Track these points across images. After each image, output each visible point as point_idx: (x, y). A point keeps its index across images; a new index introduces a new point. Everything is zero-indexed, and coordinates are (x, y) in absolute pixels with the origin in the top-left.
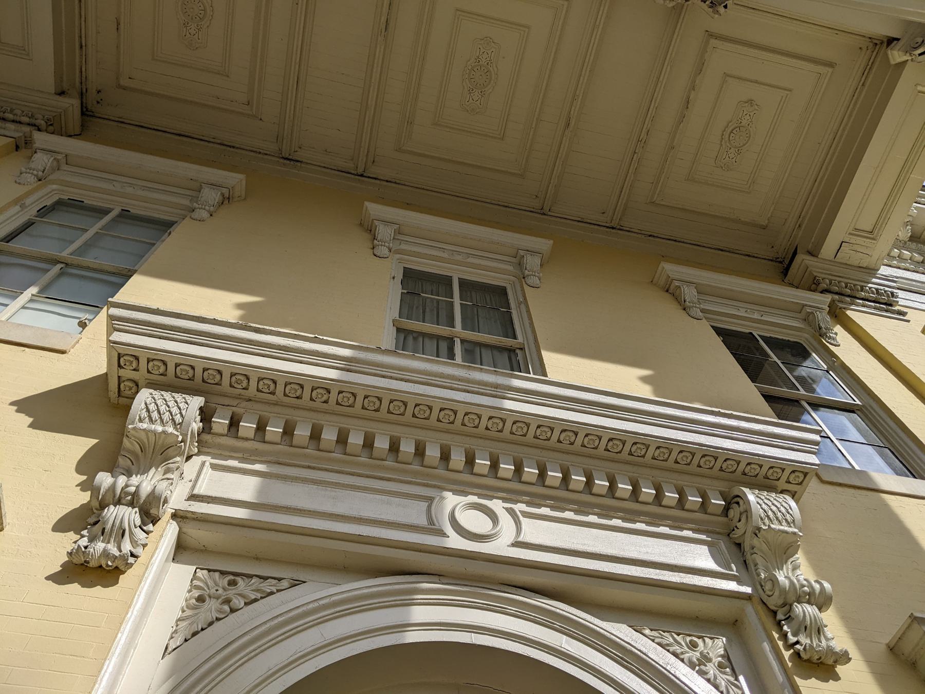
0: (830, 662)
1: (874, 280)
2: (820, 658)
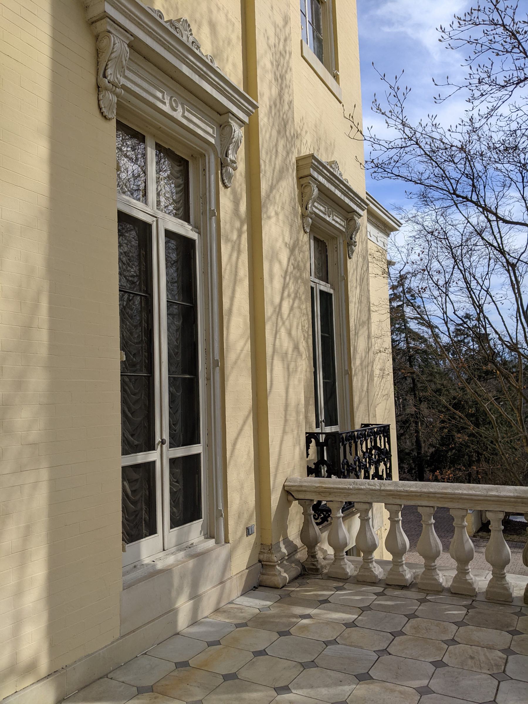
1: (383, 447)
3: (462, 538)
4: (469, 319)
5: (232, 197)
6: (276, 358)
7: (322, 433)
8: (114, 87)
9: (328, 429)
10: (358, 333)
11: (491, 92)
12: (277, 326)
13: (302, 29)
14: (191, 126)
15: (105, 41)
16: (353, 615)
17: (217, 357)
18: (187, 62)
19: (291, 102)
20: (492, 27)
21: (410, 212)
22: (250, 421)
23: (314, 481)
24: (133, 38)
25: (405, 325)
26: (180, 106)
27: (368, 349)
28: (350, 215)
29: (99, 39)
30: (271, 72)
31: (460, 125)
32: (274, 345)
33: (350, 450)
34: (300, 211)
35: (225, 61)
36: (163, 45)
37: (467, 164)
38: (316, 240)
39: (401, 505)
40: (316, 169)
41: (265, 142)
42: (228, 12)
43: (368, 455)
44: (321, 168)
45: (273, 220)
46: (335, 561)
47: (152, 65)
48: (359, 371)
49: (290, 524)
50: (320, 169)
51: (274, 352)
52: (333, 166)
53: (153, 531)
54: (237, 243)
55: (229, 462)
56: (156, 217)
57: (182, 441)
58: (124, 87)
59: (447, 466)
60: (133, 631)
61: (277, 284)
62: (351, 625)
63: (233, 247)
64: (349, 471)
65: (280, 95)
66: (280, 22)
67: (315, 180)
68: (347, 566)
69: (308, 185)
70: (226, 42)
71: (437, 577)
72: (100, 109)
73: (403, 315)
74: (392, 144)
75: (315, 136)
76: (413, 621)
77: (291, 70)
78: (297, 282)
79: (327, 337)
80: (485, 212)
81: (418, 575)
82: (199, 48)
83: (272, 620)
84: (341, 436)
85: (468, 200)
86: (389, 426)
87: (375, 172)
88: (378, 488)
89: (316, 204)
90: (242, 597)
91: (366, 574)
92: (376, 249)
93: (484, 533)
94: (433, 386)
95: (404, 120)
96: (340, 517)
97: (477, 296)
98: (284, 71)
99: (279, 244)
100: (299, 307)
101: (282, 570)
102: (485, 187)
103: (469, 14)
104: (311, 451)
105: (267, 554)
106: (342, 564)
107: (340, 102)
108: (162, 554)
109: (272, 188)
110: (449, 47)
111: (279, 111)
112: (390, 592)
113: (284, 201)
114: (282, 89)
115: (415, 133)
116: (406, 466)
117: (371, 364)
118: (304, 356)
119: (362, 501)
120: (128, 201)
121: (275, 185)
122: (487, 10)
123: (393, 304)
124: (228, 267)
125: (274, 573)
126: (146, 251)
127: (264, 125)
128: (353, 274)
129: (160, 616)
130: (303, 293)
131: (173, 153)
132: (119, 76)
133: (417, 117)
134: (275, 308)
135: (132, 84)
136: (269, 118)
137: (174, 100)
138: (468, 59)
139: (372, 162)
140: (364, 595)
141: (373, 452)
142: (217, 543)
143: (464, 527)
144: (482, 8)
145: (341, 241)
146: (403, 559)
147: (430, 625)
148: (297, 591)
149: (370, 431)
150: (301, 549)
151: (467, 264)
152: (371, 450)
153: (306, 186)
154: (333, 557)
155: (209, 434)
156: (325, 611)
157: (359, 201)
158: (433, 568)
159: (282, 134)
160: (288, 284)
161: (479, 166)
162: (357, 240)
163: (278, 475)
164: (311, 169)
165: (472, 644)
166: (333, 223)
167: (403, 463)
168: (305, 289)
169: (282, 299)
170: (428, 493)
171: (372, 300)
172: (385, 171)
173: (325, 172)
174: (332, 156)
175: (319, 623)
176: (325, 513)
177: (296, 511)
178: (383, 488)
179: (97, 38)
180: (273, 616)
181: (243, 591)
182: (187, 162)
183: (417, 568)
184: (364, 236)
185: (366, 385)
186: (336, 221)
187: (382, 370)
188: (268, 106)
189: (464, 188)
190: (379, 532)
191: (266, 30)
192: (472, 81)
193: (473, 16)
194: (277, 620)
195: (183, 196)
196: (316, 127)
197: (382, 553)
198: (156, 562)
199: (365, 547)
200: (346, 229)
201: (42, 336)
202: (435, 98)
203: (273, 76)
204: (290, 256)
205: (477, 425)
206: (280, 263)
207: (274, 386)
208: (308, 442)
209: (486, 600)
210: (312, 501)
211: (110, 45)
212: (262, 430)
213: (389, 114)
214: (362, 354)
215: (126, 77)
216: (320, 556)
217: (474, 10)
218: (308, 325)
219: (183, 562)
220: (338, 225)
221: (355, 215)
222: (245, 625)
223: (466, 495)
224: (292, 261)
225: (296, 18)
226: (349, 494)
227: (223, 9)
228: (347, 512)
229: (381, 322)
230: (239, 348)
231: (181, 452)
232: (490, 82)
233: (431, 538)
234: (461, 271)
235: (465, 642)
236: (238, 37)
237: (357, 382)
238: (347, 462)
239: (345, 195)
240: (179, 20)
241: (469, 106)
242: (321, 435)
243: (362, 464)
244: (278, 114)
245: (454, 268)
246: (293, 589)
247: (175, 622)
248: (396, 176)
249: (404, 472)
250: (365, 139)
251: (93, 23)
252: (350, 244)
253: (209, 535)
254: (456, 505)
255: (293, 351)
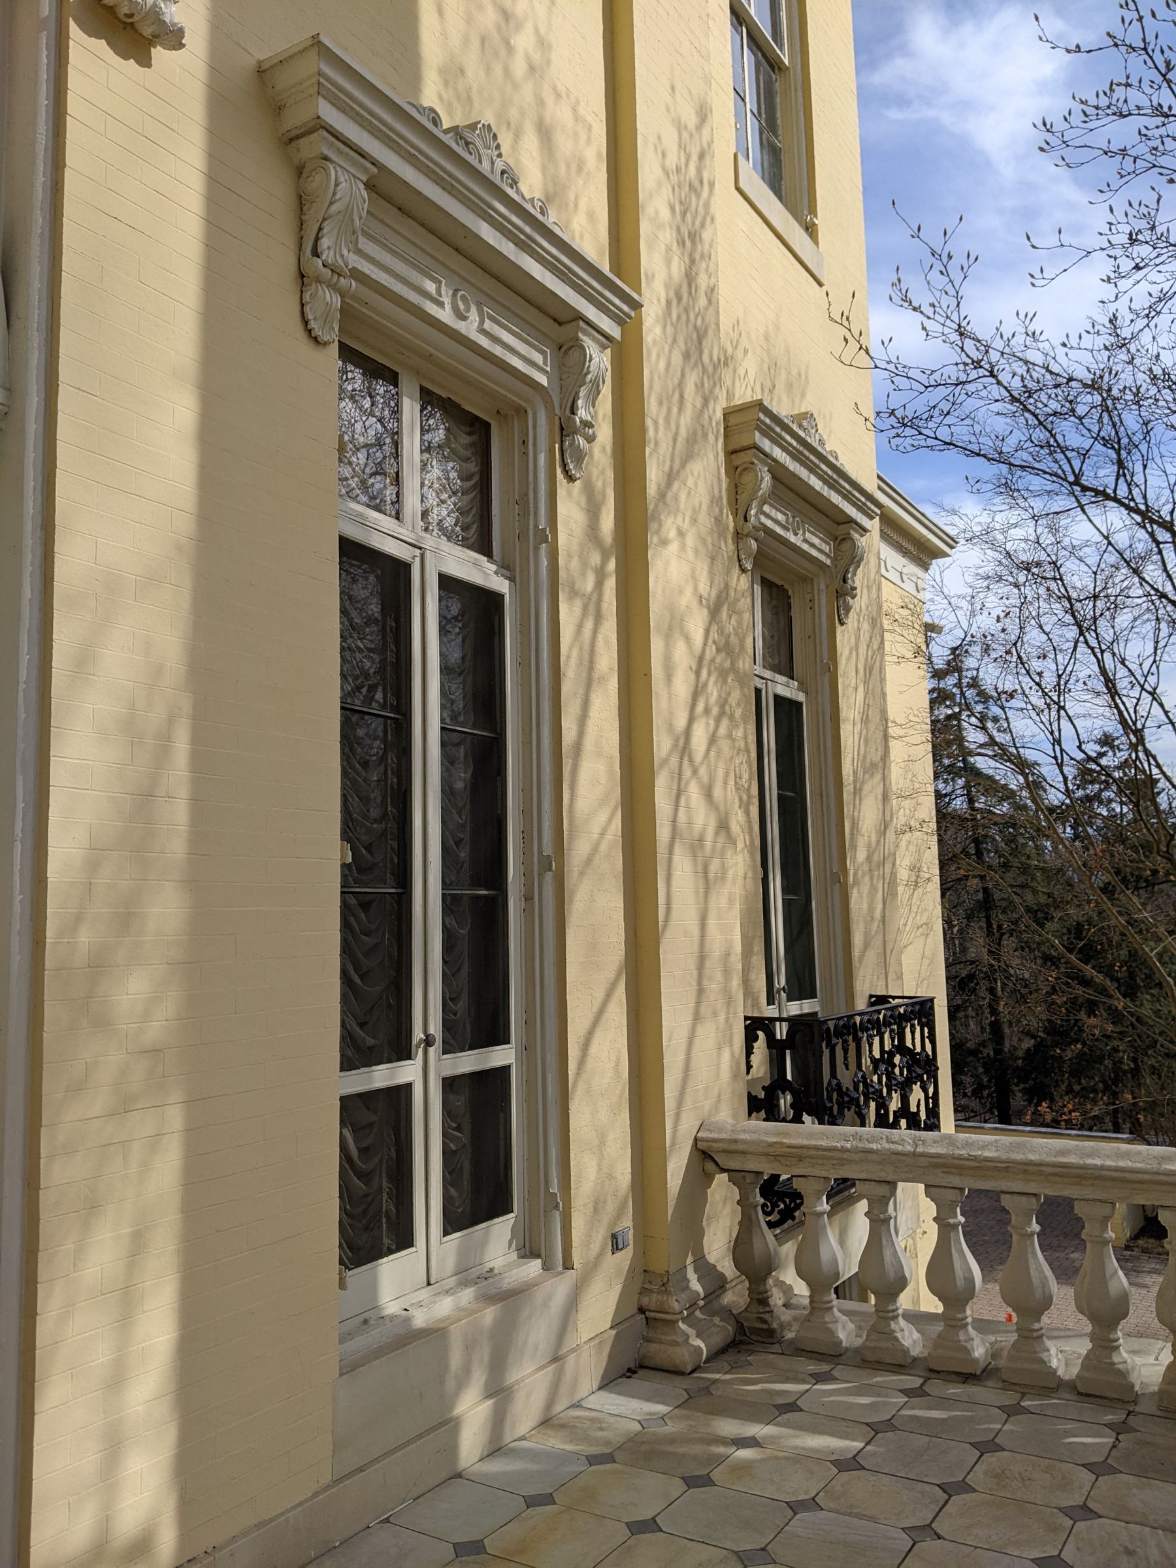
0: (147, 31)
1: (918, 1049)
2: (131, 16)
3: (1104, 1267)
4: (1112, 747)
5: (583, 500)
6: (678, 850)
7: (781, 1019)
8: (336, 276)
9: (794, 1008)
10: (861, 790)
11: (1158, 261)
12: (680, 779)
13: (737, 129)
14: (498, 351)
15: (318, 178)
16: (853, 1440)
17: (548, 850)
18: (490, 216)
19: (712, 290)
20: (1159, 120)
21: (977, 520)
22: (621, 992)
23: (761, 1129)
24: (375, 170)
25: (964, 761)
26: (474, 309)
27: (884, 826)
28: (841, 530)
29: (304, 175)
30: (671, 227)
31: (1088, 332)
32: (674, 821)
33: (846, 1058)
34: (732, 524)
35: (572, 205)
36: (438, 181)
37: (1106, 419)
38: (766, 584)
39: (962, 1190)
40: (766, 432)
41: (656, 378)
42: (578, 102)
43: (886, 1069)
44: (778, 429)
45: (674, 547)
46: (811, 1313)
47: (415, 224)
48: (864, 875)
49: (709, 1225)
50: (776, 433)
51: (673, 838)
52: (805, 423)
53: (405, 1241)
54: (594, 599)
55: (574, 1087)
56: (420, 548)
57: (468, 1035)
58: (356, 274)
59: (1063, 1081)
60: (361, 1469)
61: (682, 687)
62: (849, 1464)
63: (585, 608)
64: (842, 1106)
65: (690, 278)
66: (690, 118)
67: (766, 456)
68: (840, 1326)
69: (749, 467)
70: (574, 167)
71: (1044, 1355)
72: (306, 322)
73: (960, 740)
74: (936, 376)
75: (766, 360)
76: (990, 1459)
77: (712, 220)
78: (725, 681)
79: (791, 798)
80: (1148, 525)
81: (1002, 1349)
82: (516, 183)
83: (669, 1449)
84: (825, 1027)
85: (1107, 497)
86: (932, 1000)
87: (898, 436)
88: (909, 1148)
89: (766, 508)
90: (601, 1393)
91: (884, 1344)
92: (900, 602)
93: (1151, 1241)
94: (1029, 897)
95: (964, 324)
96: (822, 1214)
97: (1131, 711)
98: (697, 223)
99: (687, 599)
100: (730, 736)
101: (691, 1332)
102: (1145, 467)
103: (1105, 94)
104: (756, 1059)
105: (658, 1293)
106: (827, 1319)
107: (820, 284)
108: (424, 1294)
109: (671, 477)
110: (1061, 163)
111: (686, 310)
112: (936, 1387)
113: (697, 506)
114: (693, 261)
115: (987, 351)
116: (967, 1080)
117: (891, 860)
118: (740, 845)
119: (874, 1177)
120: (361, 515)
121: (678, 472)
122: (1145, 85)
123: (936, 712)
124: (575, 653)
125: (674, 1338)
126: (397, 621)
127: (654, 342)
128: (849, 658)
129: (420, 1436)
130: (738, 705)
131: (457, 406)
132: (345, 252)
133: (993, 310)
134: (677, 740)
135: (372, 267)
136: (664, 328)
137: (463, 296)
138: (1106, 189)
139: (892, 413)
140: (879, 1395)
141: (897, 1059)
142: (546, 1267)
143: (1106, 1242)
144: (1134, 80)
145: (823, 587)
146: (968, 1312)
147: (1030, 1469)
148: (724, 1382)
149: (889, 1013)
150: (733, 1284)
151: (1107, 635)
152: (891, 1054)
153: (745, 469)
154: (806, 1301)
155: (529, 1022)
156: (791, 1431)
157: (863, 499)
158: (1035, 1334)
159: (692, 361)
160: (705, 685)
161: (1131, 420)
162: (857, 584)
163: (684, 1116)
164: (757, 434)
165: (1128, 1518)
166: (805, 547)
167: (962, 1073)
168: (743, 694)
169: (691, 720)
170: (1026, 1164)
171: (891, 715)
172: (920, 433)
173: (788, 438)
174: (801, 401)
175: (777, 1458)
176: (788, 1201)
177: (722, 1195)
178: (920, 1149)
179: (299, 171)
180: (672, 1440)
181: (604, 1377)
182: (487, 425)
183: (998, 1332)
184: (872, 576)
185: (880, 906)
186: (811, 542)
187: (915, 869)
188: (663, 301)
189: (1102, 473)
190: (910, 1241)
191: (659, 138)
192: (1115, 239)
193: (1115, 96)
194: (681, 1450)
195: (478, 499)
196: (767, 339)
197: (920, 1297)
198: (414, 1312)
199: (880, 1281)
200: (833, 560)
201: (177, 813)
202: (1032, 276)
203: (674, 235)
204: (710, 623)
205: (1131, 992)
206: (688, 639)
207: (675, 913)
208: (750, 1039)
209: (1159, 1413)
210: (759, 1174)
211: (328, 186)
212: (647, 1021)
213: (929, 311)
214: (869, 837)
215: (359, 252)
216: (777, 1299)
217: (1118, 85)
218: (747, 774)
219: (473, 1312)
220: (814, 553)
221: (854, 529)
222: (609, 1458)
223: (1109, 1169)
224: (714, 635)
225: (724, 108)
226: (842, 1162)
227: (568, 96)
228: (838, 1198)
229: (911, 759)
230: (596, 830)
231: (468, 1062)
232: (1154, 237)
233: (1032, 1267)
234: (1092, 649)
235: (1113, 1515)
236: (599, 154)
237: (859, 901)
238: (839, 1085)
239: (831, 487)
240: (473, 127)
241: (1109, 291)
242: (778, 1023)
243: (871, 1090)
244: (684, 317)
245: (1076, 642)
246: (717, 1376)
247: (452, 1449)
248: (946, 443)
249: (965, 1095)
250: (876, 367)
251: (291, 140)
252: (843, 592)
253: (529, 1249)
254: (1088, 1193)
255: (717, 834)
